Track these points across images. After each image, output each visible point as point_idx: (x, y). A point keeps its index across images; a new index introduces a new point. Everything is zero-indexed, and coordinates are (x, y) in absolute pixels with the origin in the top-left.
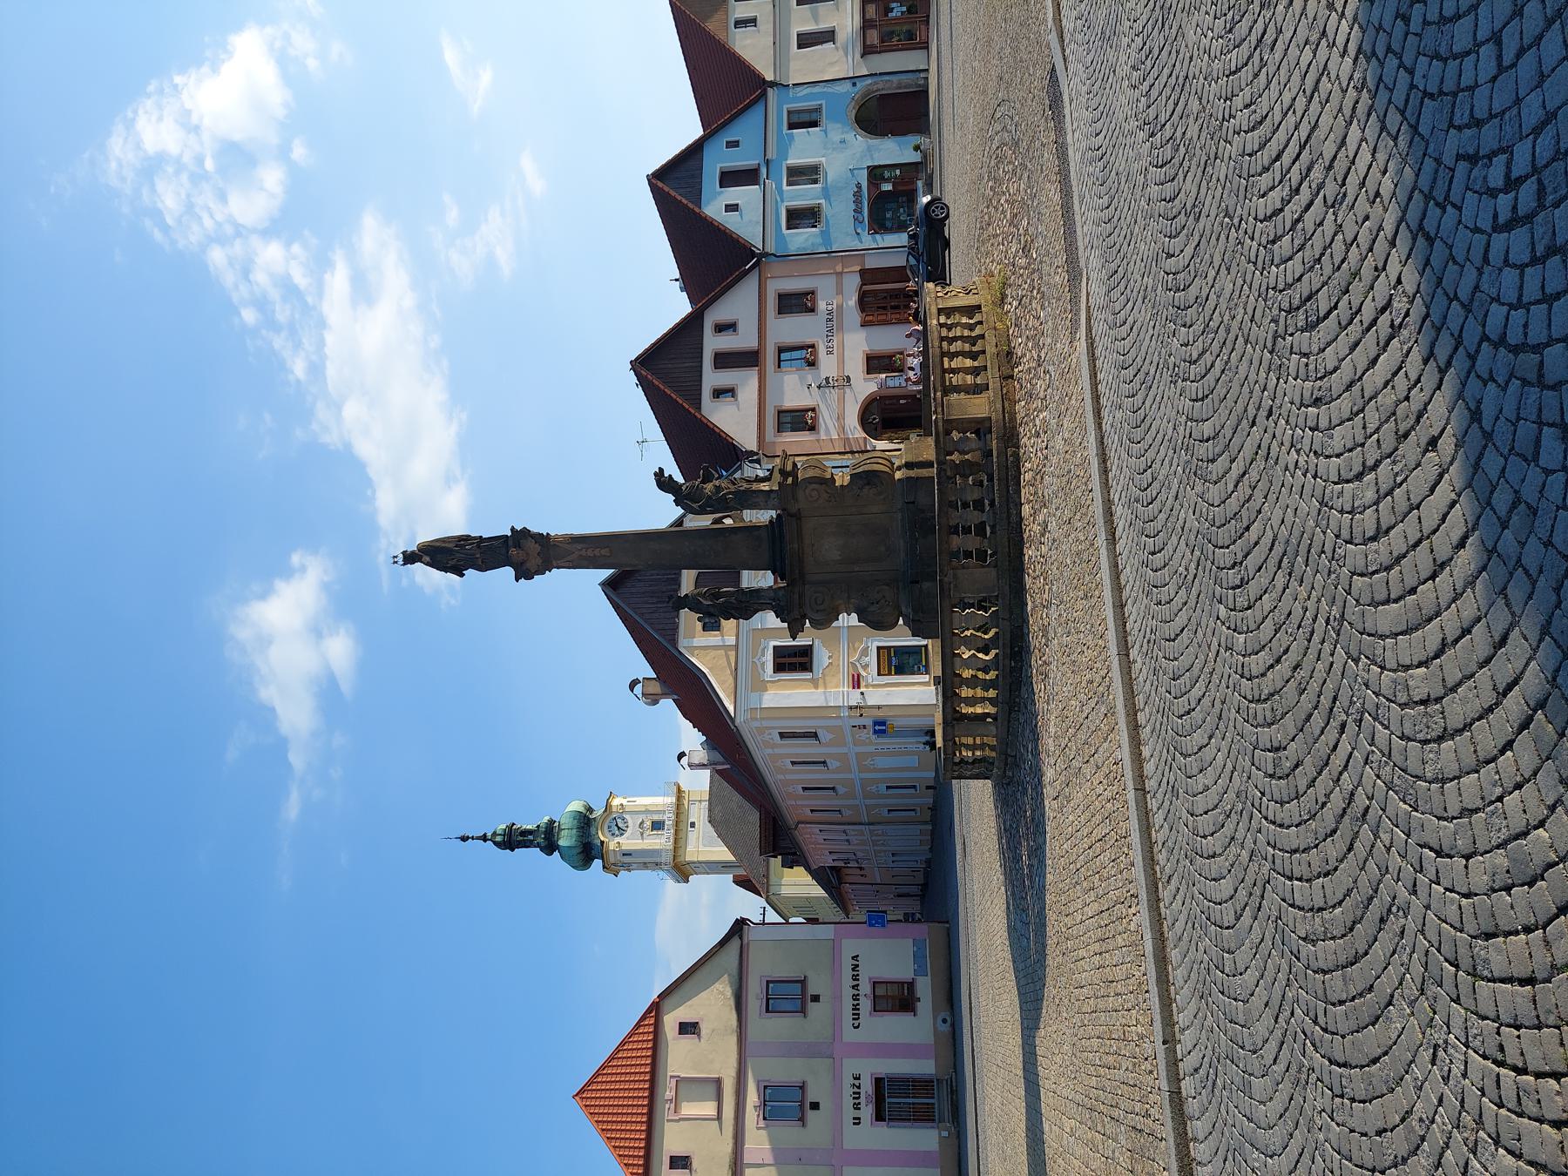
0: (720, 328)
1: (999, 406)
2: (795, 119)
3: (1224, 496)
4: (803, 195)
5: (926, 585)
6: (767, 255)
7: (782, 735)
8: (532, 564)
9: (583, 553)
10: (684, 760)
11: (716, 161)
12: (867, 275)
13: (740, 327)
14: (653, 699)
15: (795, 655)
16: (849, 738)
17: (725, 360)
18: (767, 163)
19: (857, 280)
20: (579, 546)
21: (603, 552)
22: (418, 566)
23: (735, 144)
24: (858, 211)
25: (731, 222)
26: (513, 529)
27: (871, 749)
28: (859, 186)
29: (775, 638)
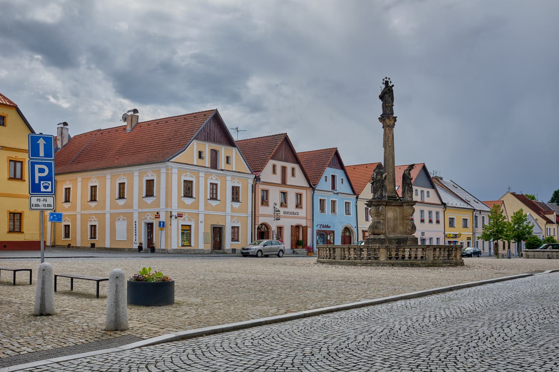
0: (293, 169)
4: (328, 207)
12: (305, 229)
13: (293, 178)
15: (476, 224)
17: (215, 154)
18: (337, 194)
19: (304, 225)
22: (383, 86)
24: (323, 226)
25: (323, 178)
28: (329, 227)
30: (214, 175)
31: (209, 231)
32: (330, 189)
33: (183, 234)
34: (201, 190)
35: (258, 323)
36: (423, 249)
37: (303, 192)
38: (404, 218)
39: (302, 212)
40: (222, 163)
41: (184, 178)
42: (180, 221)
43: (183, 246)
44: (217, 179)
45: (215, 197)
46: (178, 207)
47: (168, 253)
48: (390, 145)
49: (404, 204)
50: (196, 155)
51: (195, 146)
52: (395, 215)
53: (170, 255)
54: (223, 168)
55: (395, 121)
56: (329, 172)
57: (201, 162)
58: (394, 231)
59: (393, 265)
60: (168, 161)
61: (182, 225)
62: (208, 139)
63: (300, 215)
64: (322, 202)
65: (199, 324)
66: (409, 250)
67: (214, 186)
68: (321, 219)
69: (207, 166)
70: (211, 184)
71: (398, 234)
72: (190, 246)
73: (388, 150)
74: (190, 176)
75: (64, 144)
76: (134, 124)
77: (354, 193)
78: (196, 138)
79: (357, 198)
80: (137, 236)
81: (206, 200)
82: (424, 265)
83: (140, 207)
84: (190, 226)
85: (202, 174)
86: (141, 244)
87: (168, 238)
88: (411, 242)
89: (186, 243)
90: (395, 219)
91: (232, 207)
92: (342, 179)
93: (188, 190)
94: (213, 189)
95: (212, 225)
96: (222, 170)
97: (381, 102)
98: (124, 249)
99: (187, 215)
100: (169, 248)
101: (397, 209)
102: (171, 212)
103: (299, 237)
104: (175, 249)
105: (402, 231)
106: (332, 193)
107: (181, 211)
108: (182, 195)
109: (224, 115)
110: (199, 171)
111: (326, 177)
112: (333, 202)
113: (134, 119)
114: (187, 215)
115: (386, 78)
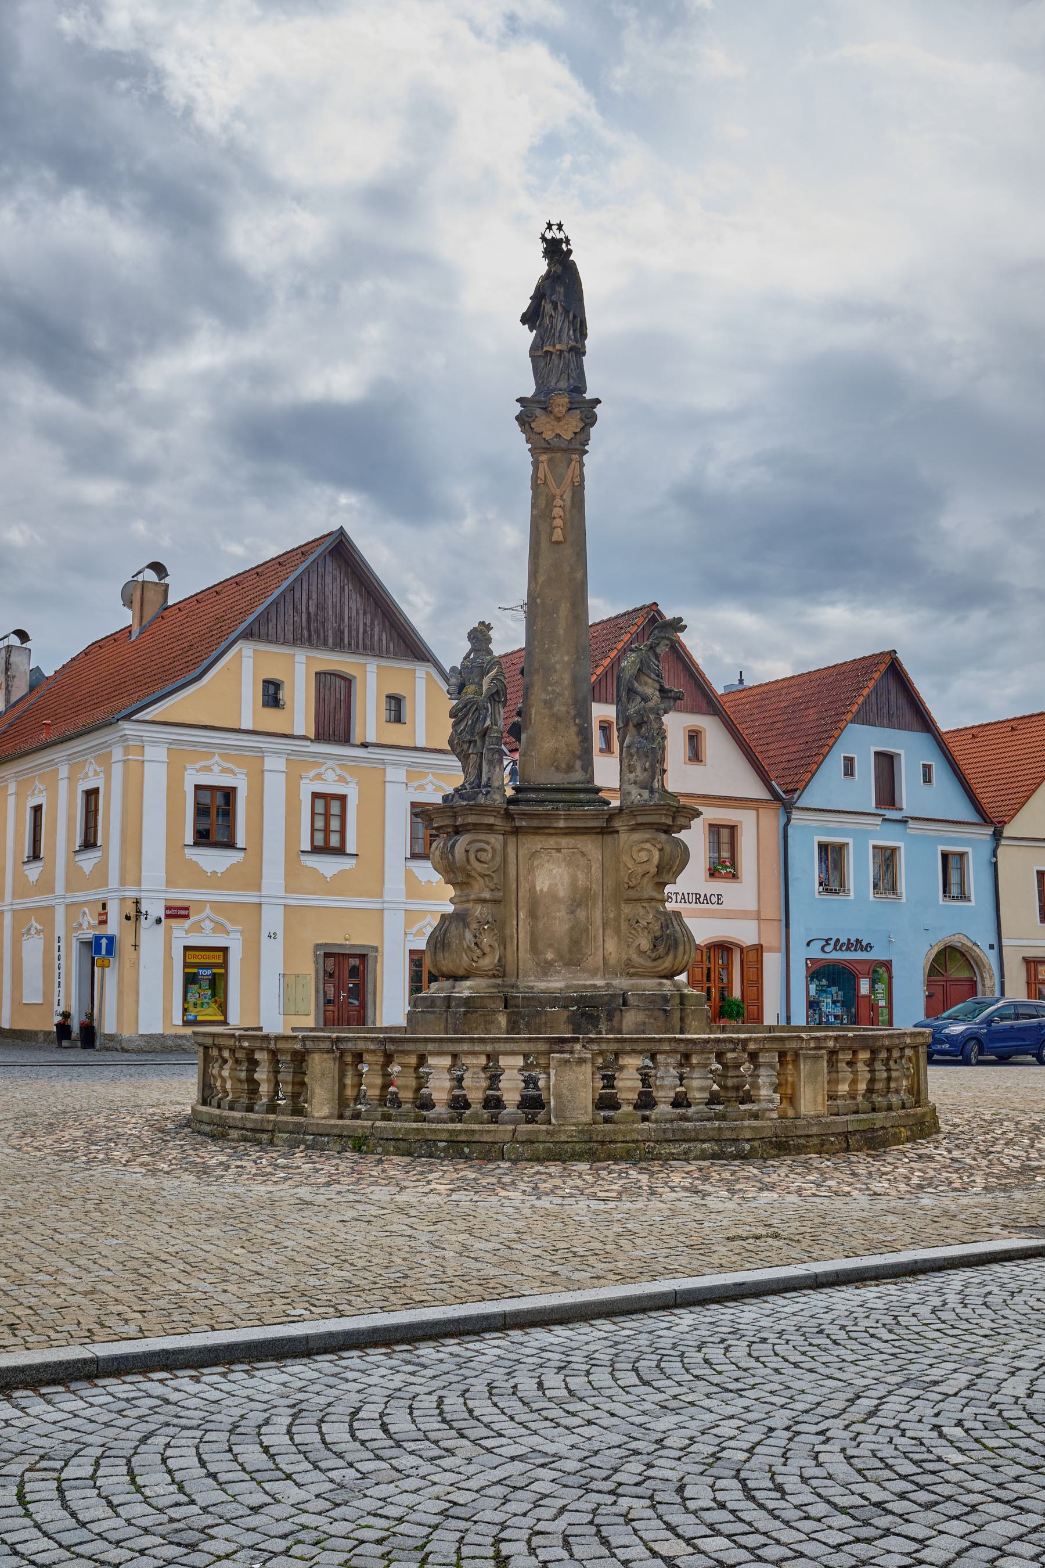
0: (694, 738)
1: (814, 1130)
2: (953, 862)
3: (50, 1528)
4: (860, 869)
5: (503, 1020)
6: (788, 814)
7: (92, 795)
8: (542, 423)
9: (558, 502)
10: (15, 641)
11: (911, 750)
13: (695, 768)
14: (133, 594)
16: (81, 897)
18: (904, 821)
20: (568, 496)
21: (558, 535)
22: (541, 266)
23: (927, 779)
24: (838, 946)
25: (834, 764)
26: (598, 401)
27: (60, 930)
28: (868, 947)
29: (250, 788)
30: (330, 763)
31: (308, 968)
32: (871, 806)
33: (190, 980)
34: (274, 816)
35: (375, 1330)
36: (782, 1055)
37: (746, 821)
38: (625, 893)
39: (741, 894)
40: (369, 719)
41: (193, 778)
42: (176, 933)
43: (186, 1023)
44: (342, 779)
45: (334, 841)
46: (170, 882)
47: (125, 1050)
48: (558, 535)
49: (617, 824)
50: (250, 693)
51: (248, 665)
52: (582, 881)
53: (126, 1056)
54: (371, 738)
55: (590, 420)
56: (861, 742)
57: (272, 719)
58: (573, 956)
59: (360, 1144)
60: (127, 717)
61: (186, 948)
62: (311, 635)
63: (728, 904)
64: (831, 856)
65: (488, 1290)
66: (447, 1061)
67: (330, 805)
68: (852, 917)
69: (299, 731)
70: (315, 795)
71: (594, 973)
72: (225, 1023)
73: (545, 563)
74: (224, 770)
75: (14, 699)
76: (150, 612)
77: (984, 818)
78: (249, 635)
79: (997, 836)
80: (62, 989)
81: (293, 855)
82: (527, 1151)
83: (69, 887)
84: (225, 950)
85: (275, 764)
86: (66, 1015)
87: (130, 991)
88: (641, 1017)
89: (210, 1013)
90: (580, 900)
91: (409, 875)
92: (927, 768)
93: (215, 818)
94: (327, 816)
95: (318, 946)
96: (364, 745)
97: (527, 336)
98: (36, 1033)
99: (208, 911)
100: (127, 1033)
101: (590, 846)
102: (137, 902)
103: (729, 986)
104: (151, 1036)
105: (613, 960)
106: (878, 821)
107: (180, 896)
108: (189, 839)
109: (377, 553)
110: (383, 762)
111: (849, 762)
112: (887, 858)
113: (150, 594)
114: (208, 911)
115: (550, 226)
